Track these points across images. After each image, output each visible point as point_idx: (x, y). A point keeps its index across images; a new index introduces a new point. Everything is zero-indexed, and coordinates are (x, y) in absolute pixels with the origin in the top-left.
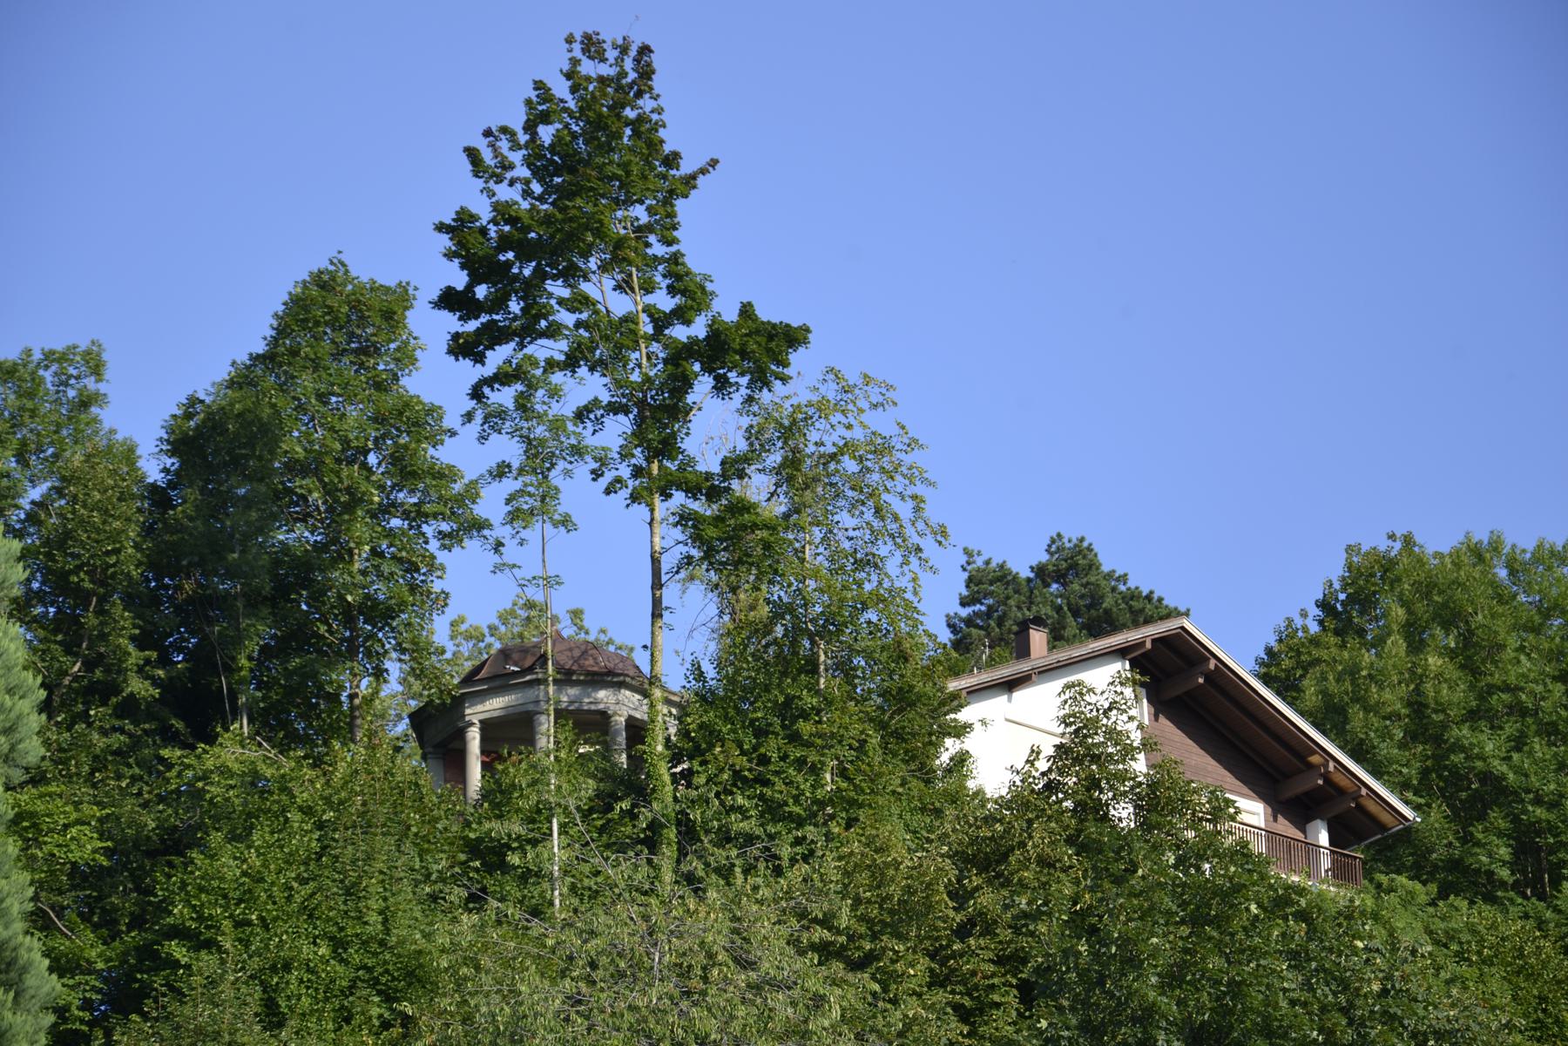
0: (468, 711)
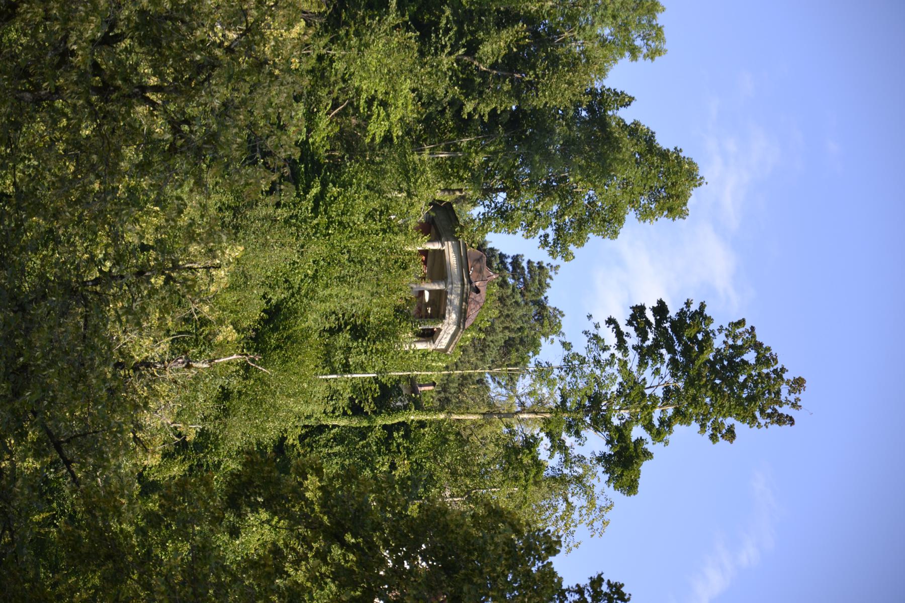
0: (450, 243)
